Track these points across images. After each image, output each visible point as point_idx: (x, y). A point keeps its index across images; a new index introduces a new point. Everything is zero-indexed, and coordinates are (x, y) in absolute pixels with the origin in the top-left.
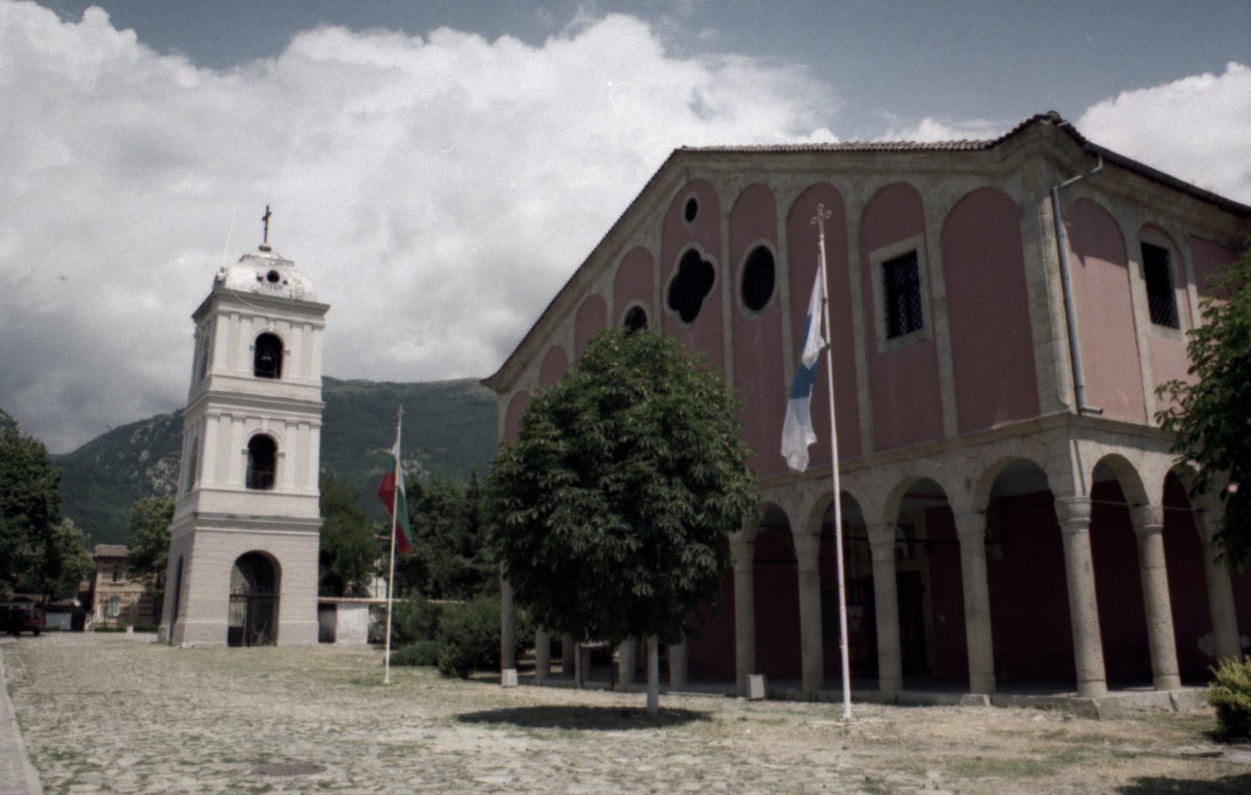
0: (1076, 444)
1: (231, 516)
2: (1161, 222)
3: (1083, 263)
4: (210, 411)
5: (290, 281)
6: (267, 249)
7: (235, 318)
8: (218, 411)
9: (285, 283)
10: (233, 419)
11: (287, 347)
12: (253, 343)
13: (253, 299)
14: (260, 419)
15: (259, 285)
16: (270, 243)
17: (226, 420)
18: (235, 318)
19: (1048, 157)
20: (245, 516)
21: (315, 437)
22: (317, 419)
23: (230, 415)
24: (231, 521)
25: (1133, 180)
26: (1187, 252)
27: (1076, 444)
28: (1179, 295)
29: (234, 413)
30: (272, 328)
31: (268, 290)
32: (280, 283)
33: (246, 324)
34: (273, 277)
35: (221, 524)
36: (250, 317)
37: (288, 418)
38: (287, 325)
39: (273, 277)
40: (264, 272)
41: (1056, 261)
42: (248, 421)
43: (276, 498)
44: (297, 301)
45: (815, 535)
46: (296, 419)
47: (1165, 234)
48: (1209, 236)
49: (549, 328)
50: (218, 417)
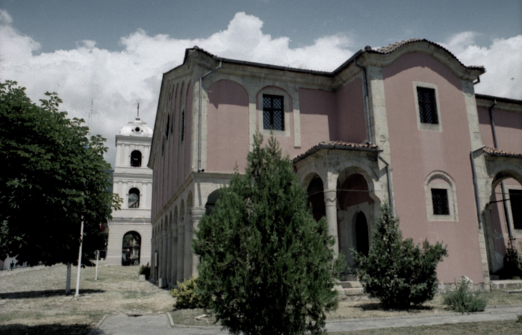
0: (199, 185)
1: (122, 218)
2: (277, 84)
3: (217, 107)
4: (114, 180)
5: (144, 130)
6: (138, 119)
7: (123, 146)
8: (118, 180)
9: (142, 131)
10: (123, 182)
11: (143, 155)
12: (130, 154)
13: (130, 138)
14: (133, 182)
15: (132, 133)
16: (140, 117)
17: (120, 183)
18: (123, 146)
19: (200, 65)
20: (127, 218)
21: (150, 186)
22: (151, 180)
23: (122, 181)
24: (122, 220)
25: (250, 69)
26: (296, 96)
27: (199, 185)
28: (287, 116)
29: (123, 181)
30: (137, 148)
31: (136, 134)
32: (140, 131)
33: (127, 147)
34: (137, 129)
35: (119, 221)
36: (129, 145)
37: (143, 181)
38: (143, 147)
39: (137, 129)
40: (134, 128)
41: (198, 108)
42: (129, 183)
43: (140, 211)
44: (146, 138)
45: (373, 207)
46: (127, 181)
47: (282, 89)
48: (316, 88)
49: (155, 145)
50: (117, 182)
